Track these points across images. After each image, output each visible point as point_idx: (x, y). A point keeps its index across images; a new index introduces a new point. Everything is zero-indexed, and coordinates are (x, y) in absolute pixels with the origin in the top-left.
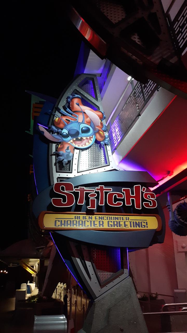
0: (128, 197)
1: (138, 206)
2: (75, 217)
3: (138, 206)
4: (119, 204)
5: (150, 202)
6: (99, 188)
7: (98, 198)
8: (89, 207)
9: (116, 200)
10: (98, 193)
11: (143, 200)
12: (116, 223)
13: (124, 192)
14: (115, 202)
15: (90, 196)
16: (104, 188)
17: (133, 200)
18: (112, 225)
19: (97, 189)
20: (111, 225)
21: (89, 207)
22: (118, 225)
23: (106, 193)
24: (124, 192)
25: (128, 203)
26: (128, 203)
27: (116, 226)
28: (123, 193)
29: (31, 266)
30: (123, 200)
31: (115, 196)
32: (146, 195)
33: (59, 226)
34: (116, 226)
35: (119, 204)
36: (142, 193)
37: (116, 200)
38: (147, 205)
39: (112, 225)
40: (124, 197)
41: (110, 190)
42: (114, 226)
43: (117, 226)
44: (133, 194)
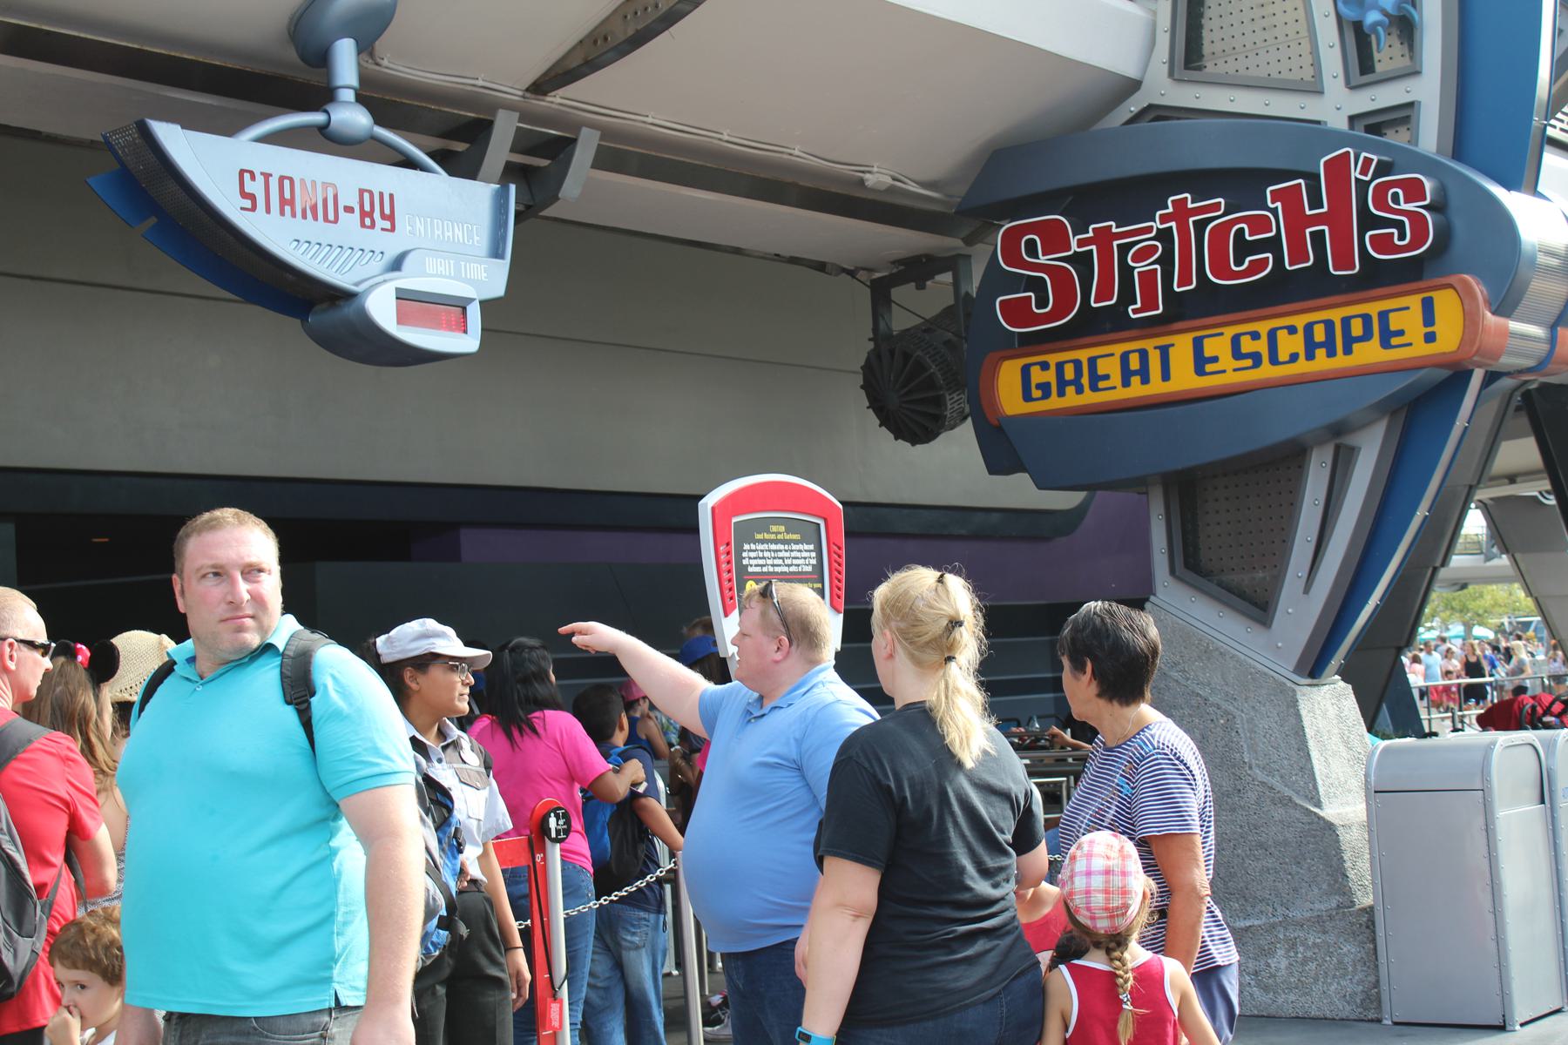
0: (1296, 221)
1: (1344, 260)
2: (1125, 358)
3: (1344, 260)
4: (1258, 266)
5: (1399, 225)
6: (1170, 210)
7: (1166, 261)
8: (1135, 311)
9: (1244, 247)
10: (1165, 236)
11: (1368, 221)
12: (1069, 373)
13: (1279, 204)
14: (1239, 262)
15: (1136, 259)
16: (1190, 206)
17: (1318, 238)
18: (1048, 384)
19: (1164, 219)
20: (1045, 388)
21: (1135, 311)
22: (1085, 381)
23: (1199, 226)
24: (1279, 204)
25: (1298, 254)
26: (1298, 254)
27: (1070, 390)
28: (1274, 211)
29: (823, 597)
30: (1273, 245)
31: (1240, 232)
32: (1382, 190)
33: (1294, 358)
34: (1070, 390)
35: (1258, 266)
36: (1363, 186)
37: (1244, 247)
38: (1383, 244)
39: (1048, 384)
40: (1279, 226)
41: (1216, 207)
42: (1061, 393)
43: (1079, 390)
44: (1316, 202)
